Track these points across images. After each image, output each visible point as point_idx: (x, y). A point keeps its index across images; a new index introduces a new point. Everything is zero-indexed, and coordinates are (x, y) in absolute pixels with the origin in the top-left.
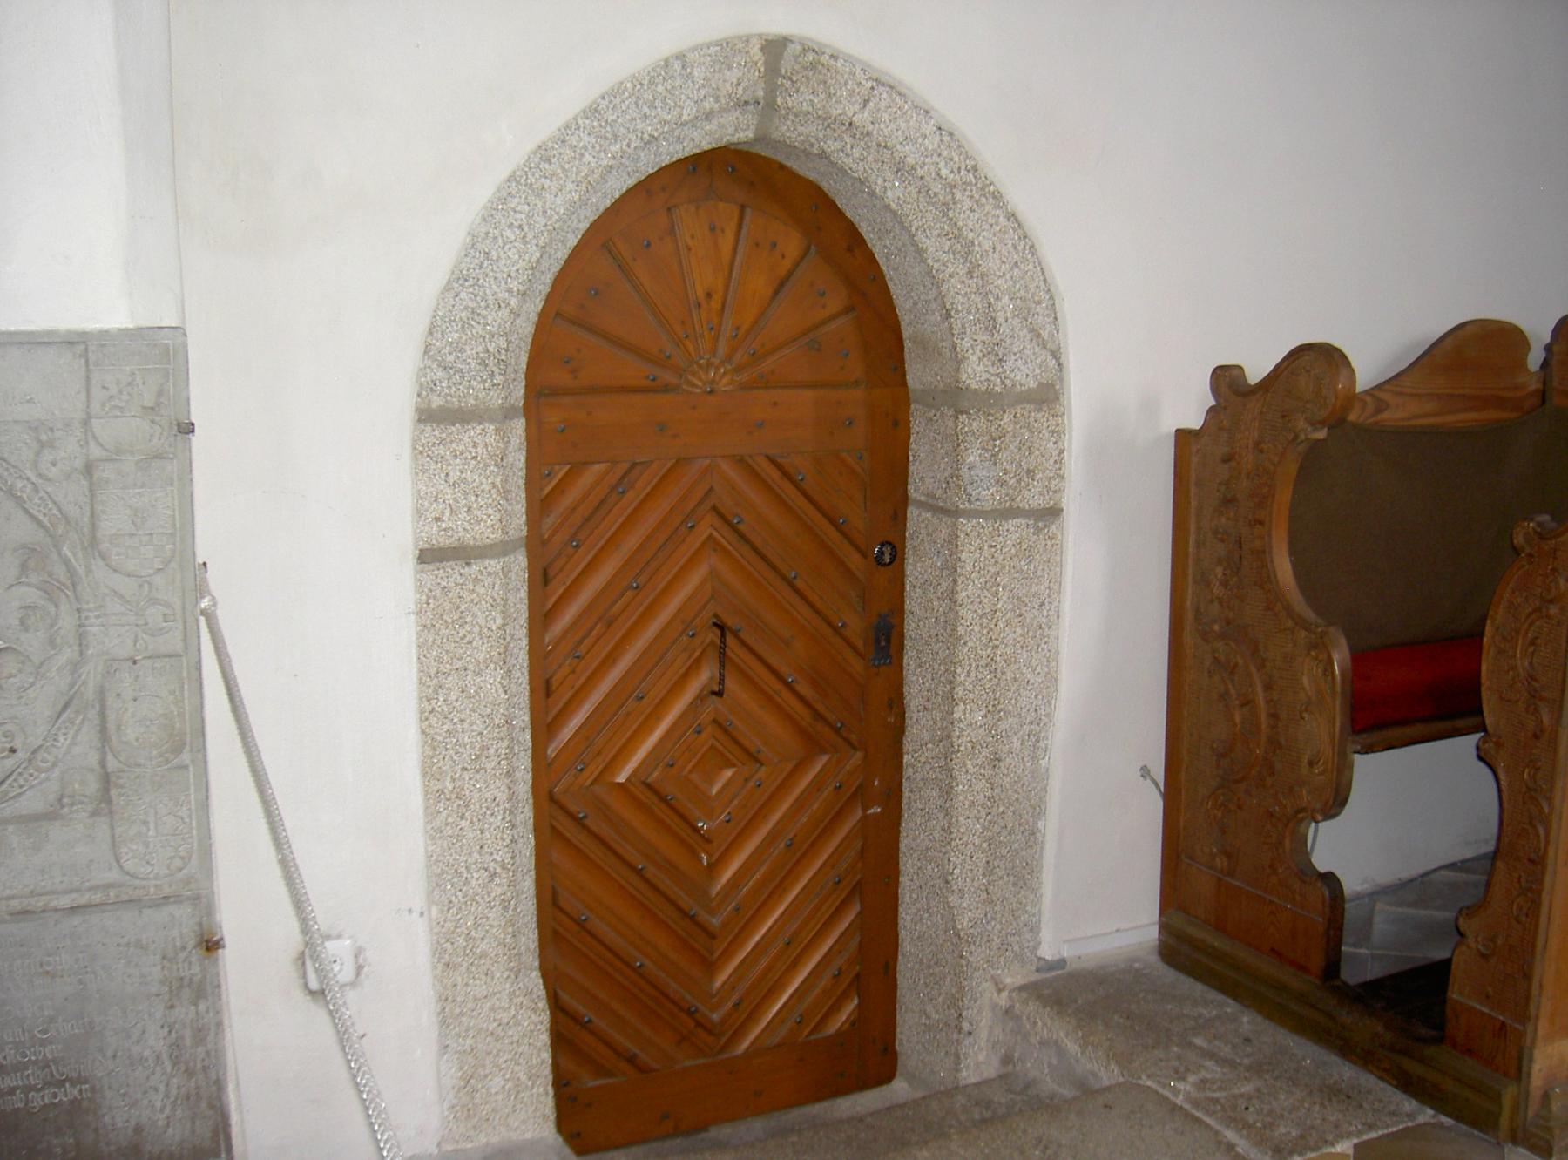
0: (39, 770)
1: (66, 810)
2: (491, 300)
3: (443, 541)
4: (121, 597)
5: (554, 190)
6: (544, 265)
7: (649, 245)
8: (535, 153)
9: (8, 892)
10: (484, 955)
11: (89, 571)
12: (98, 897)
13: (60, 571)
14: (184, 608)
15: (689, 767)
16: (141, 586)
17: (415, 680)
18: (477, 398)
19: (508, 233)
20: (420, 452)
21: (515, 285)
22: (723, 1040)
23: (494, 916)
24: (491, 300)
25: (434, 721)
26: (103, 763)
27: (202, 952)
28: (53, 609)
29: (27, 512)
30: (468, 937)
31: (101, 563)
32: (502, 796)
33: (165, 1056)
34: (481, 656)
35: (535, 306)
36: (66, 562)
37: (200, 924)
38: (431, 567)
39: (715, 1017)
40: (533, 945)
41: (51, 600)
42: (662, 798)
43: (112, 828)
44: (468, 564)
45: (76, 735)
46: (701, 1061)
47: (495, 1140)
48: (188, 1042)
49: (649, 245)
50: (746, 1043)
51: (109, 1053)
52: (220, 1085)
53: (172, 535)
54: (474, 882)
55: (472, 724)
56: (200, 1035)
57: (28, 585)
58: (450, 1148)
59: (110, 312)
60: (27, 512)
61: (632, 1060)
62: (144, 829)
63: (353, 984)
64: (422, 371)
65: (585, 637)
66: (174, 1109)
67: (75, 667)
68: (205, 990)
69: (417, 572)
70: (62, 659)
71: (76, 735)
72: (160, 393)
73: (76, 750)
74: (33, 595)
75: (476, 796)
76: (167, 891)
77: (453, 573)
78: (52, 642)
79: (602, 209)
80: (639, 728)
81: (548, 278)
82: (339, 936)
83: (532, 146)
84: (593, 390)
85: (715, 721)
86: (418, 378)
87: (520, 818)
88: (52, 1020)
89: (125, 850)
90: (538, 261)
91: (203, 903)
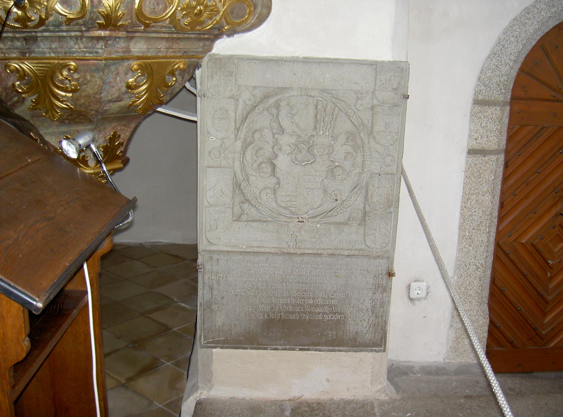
0: (344, 208)
1: (351, 222)
2: (503, 62)
3: (477, 147)
4: (378, 152)
5: (529, 24)
6: (523, 51)
7: (557, 47)
8: (524, 10)
9: (328, 247)
10: (470, 295)
11: (369, 142)
12: (357, 253)
13: (359, 141)
14: (398, 158)
15: (548, 240)
16: (385, 149)
17: (461, 195)
18: (495, 97)
19: (512, 39)
20: (473, 115)
21: (512, 58)
22: (545, 341)
23: (476, 282)
24: (503, 62)
25: (465, 210)
26: (364, 208)
27: (387, 276)
28: (355, 154)
29: (351, 121)
30: (466, 288)
31: (373, 140)
32: (485, 240)
33: (369, 310)
34: (485, 189)
35: (518, 66)
36: (362, 139)
37: (388, 267)
38: (472, 156)
39: (544, 332)
40: (487, 295)
41: (355, 151)
42: (537, 250)
43: (365, 230)
44: (485, 156)
45: (357, 198)
46: (536, 348)
47: (463, 361)
48: (378, 306)
49: (557, 47)
50: (552, 344)
51: (352, 306)
52: (386, 322)
53: (398, 133)
54: (471, 269)
55: (478, 213)
56: (382, 304)
57: (349, 145)
58: (447, 361)
59: (385, 55)
60: (351, 121)
61: (511, 343)
62: (375, 232)
63: (425, 298)
64: (477, 86)
65: (517, 189)
66: (369, 328)
67: (360, 174)
68: (386, 289)
69: (466, 157)
70: (356, 171)
71: (357, 198)
72: (399, 84)
73: (356, 202)
74: (350, 149)
75: (476, 239)
76: (379, 254)
77: (479, 159)
78: (353, 165)
79: (545, 32)
80: (533, 223)
81: (524, 56)
82: (422, 281)
83: (524, 7)
84: (533, 99)
85: (560, 225)
86: (475, 88)
87: (490, 249)
88: (335, 292)
89: (367, 238)
90: (521, 50)
91: (390, 260)
